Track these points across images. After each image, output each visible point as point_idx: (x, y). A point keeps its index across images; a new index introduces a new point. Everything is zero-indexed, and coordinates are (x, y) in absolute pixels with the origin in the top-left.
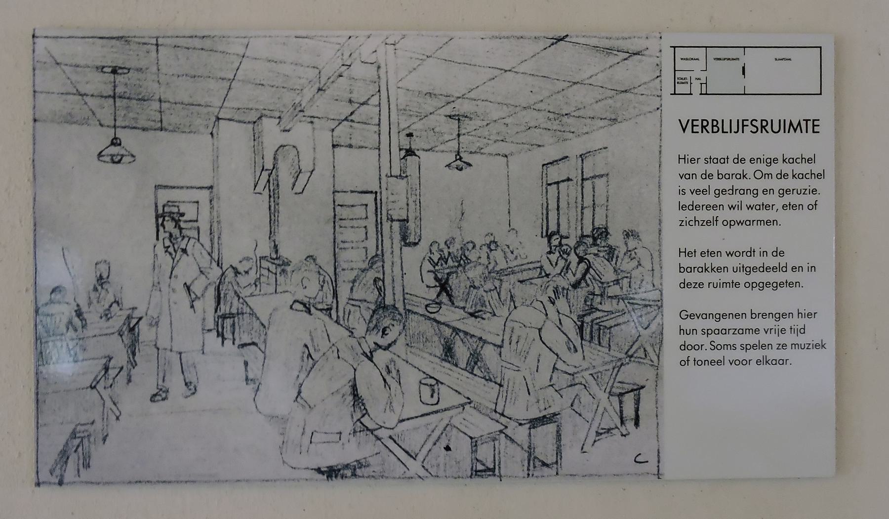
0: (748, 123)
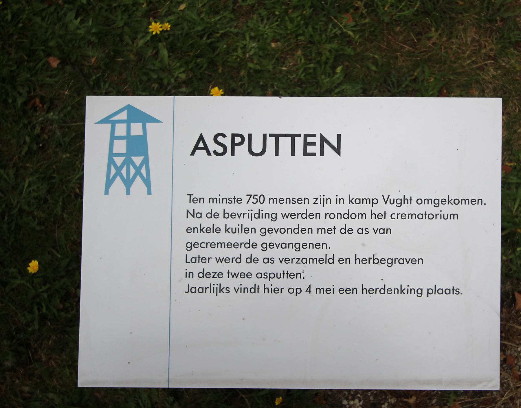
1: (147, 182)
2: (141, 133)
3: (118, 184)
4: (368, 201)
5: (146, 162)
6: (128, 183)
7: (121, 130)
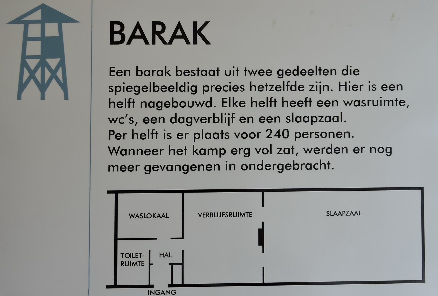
0: (225, 214)
1: (64, 86)
2: (57, 34)
3: (32, 88)
4: (215, 151)
5: (62, 64)
6: (43, 87)
7: (34, 30)
